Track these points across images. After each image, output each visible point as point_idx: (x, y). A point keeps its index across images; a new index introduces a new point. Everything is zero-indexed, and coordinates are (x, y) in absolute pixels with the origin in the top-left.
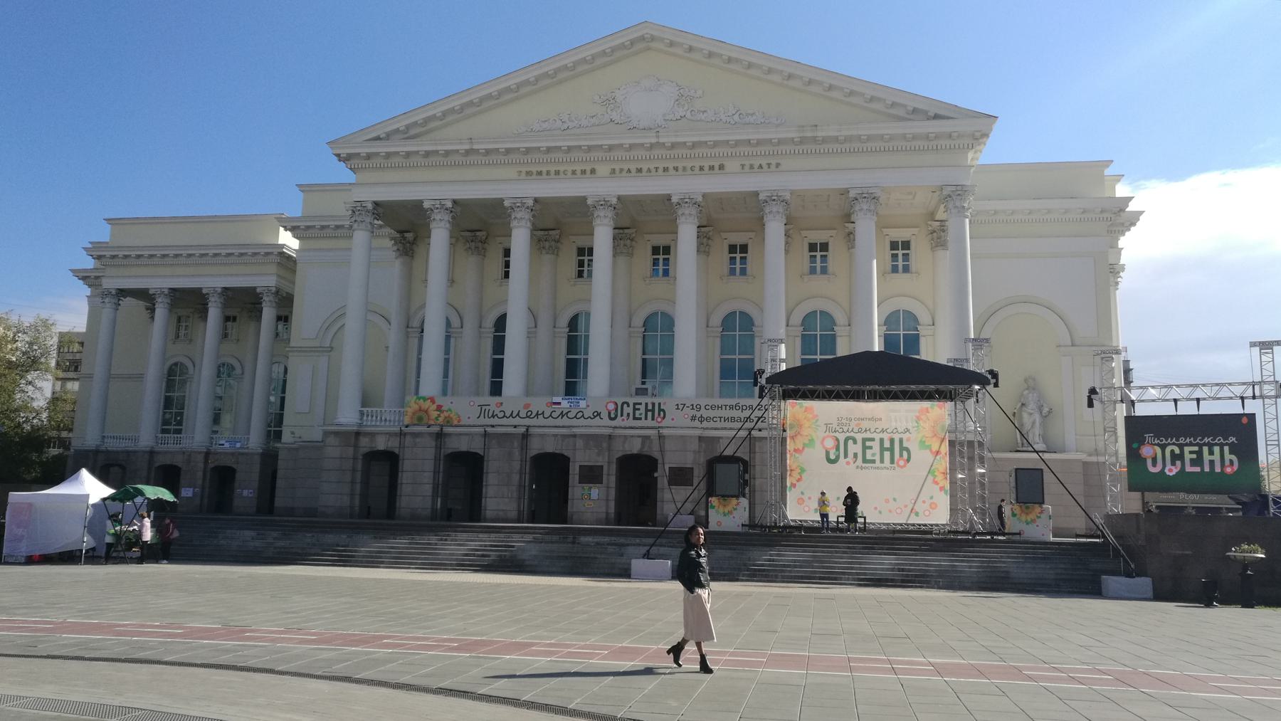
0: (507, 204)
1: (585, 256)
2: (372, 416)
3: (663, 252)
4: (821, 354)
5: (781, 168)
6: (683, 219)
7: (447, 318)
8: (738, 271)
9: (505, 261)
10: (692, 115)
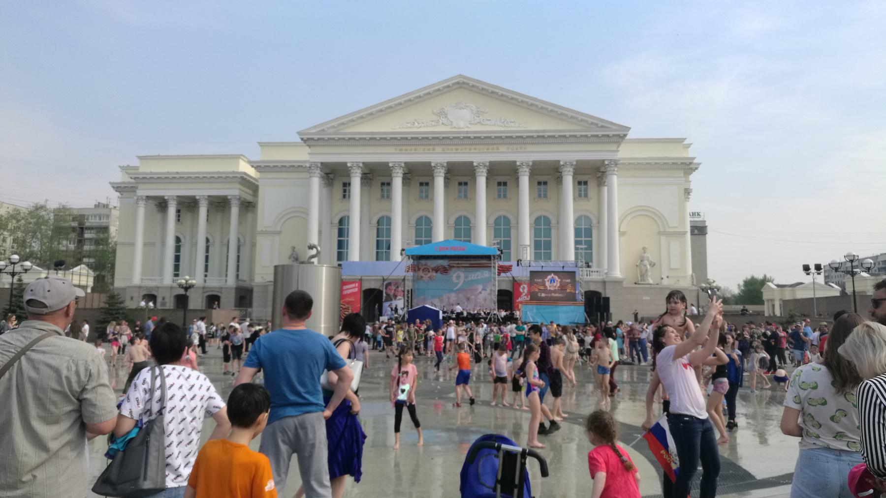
0: (606, 162)
3: (347, 185)
4: (425, 237)
6: (395, 175)
8: (542, 195)
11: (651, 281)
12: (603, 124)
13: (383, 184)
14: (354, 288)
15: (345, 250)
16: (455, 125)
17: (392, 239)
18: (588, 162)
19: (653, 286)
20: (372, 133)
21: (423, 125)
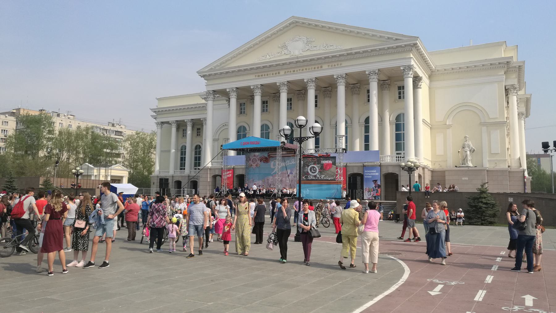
1: (401, 90)
2: (219, 163)
7: (346, 120)
9: (368, 95)
10: (311, 48)
11: (470, 164)
12: (397, 38)
14: (229, 174)
15: (402, 142)
16: (292, 53)
17: (370, 134)
18: (270, 83)
19: (470, 168)
20: (239, 67)
21: (272, 57)
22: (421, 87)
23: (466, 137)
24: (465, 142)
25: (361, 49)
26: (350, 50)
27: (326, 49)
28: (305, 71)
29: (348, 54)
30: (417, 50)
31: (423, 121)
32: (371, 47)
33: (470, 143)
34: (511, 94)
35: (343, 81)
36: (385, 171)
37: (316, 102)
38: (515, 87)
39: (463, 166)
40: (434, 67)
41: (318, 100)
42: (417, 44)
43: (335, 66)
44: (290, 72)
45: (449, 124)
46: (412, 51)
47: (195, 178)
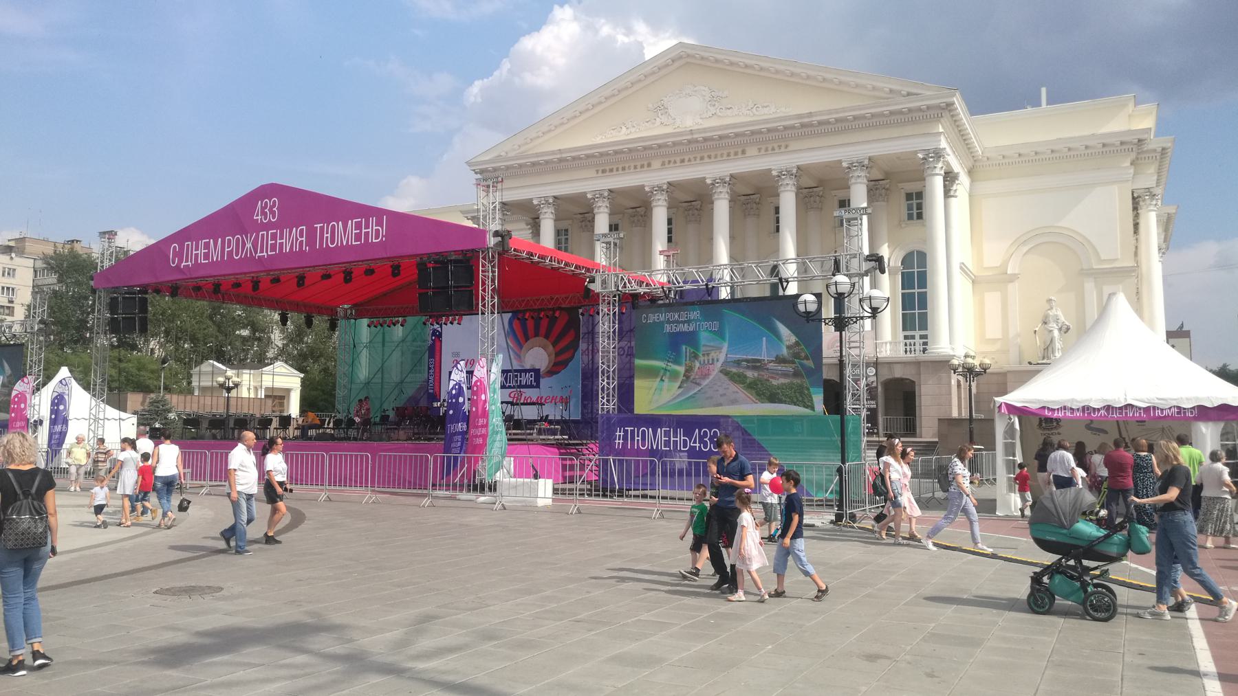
1: (913, 200)
5: (790, 149)
10: (720, 112)
13: (909, 196)
18: (819, 163)
21: (633, 130)
22: (957, 194)
23: (1050, 301)
24: (1049, 311)
25: (831, 114)
26: (808, 117)
27: (754, 115)
28: (706, 160)
29: (803, 126)
30: (952, 116)
31: (961, 268)
32: (854, 110)
33: (1059, 313)
34: (1145, 207)
35: (725, 190)
36: (886, 375)
37: (670, 231)
38: (1154, 193)
39: (1044, 361)
40: (981, 150)
41: (673, 226)
42: (953, 104)
43: (689, 160)
44: (675, 162)
45: (1014, 272)
46: (942, 120)
47: (424, 394)
